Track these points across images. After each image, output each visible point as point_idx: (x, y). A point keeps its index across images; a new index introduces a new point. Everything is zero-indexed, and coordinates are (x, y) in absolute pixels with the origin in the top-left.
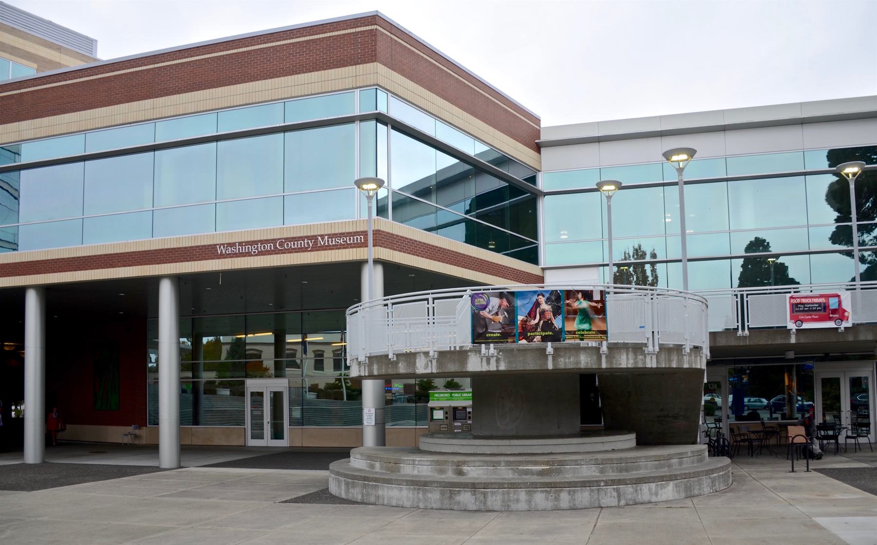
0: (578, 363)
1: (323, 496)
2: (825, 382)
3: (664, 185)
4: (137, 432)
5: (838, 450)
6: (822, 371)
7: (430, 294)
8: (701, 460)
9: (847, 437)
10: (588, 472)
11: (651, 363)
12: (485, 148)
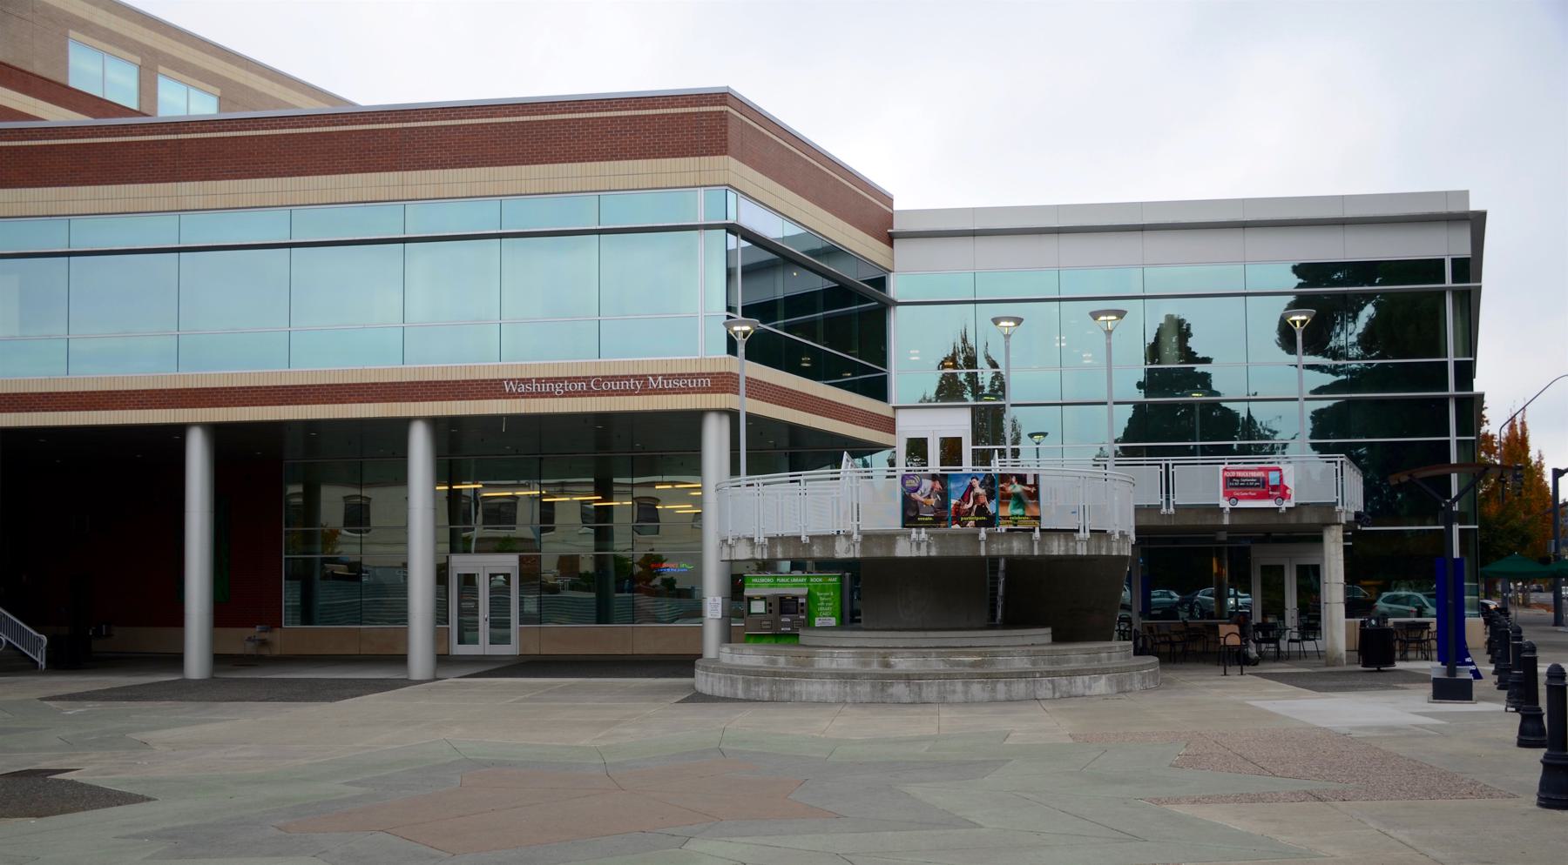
0: (1011, 549)
2: (1266, 569)
3: (1060, 300)
4: (266, 636)
5: (1279, 657)
6: (1263, 556)
8: (1127, 657)
9: (1291, 641)
10: (1020, 663)
11: (1082, 550)
12: (797, 230)
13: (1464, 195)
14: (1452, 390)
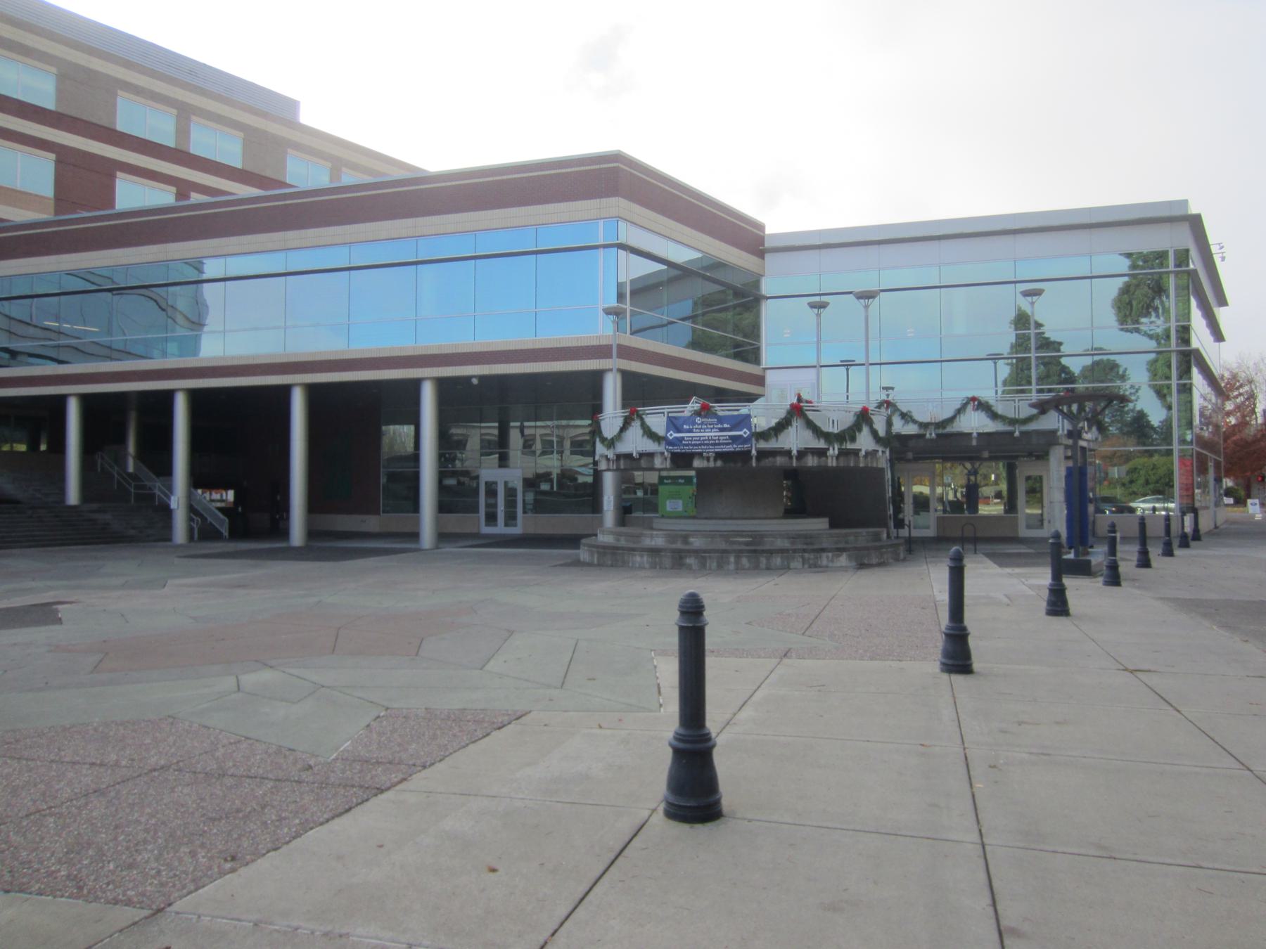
1: (577, 563)
11: (832, 463)
12: (699, 255)
13: (1184, 203)
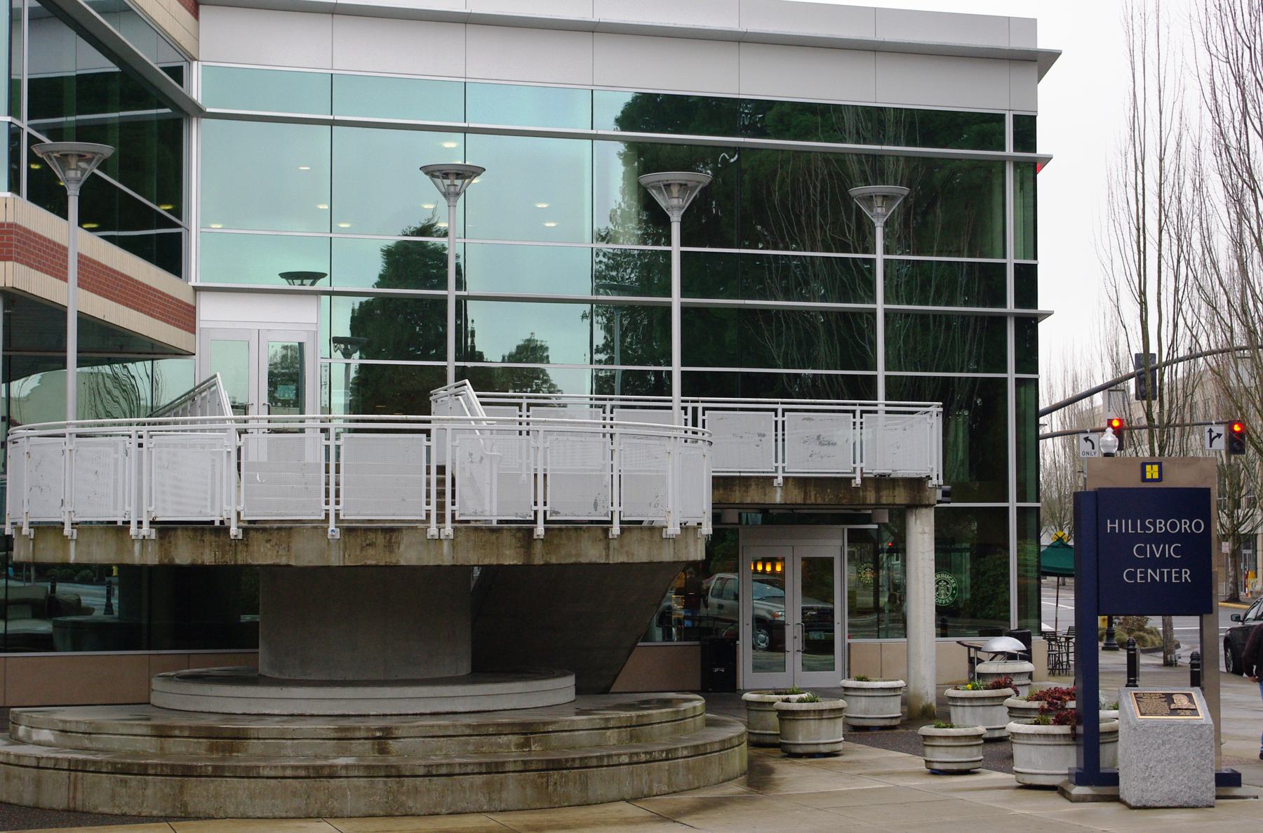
7: (780, 404)
13: (1030, 25)
14: (1011, 306)
